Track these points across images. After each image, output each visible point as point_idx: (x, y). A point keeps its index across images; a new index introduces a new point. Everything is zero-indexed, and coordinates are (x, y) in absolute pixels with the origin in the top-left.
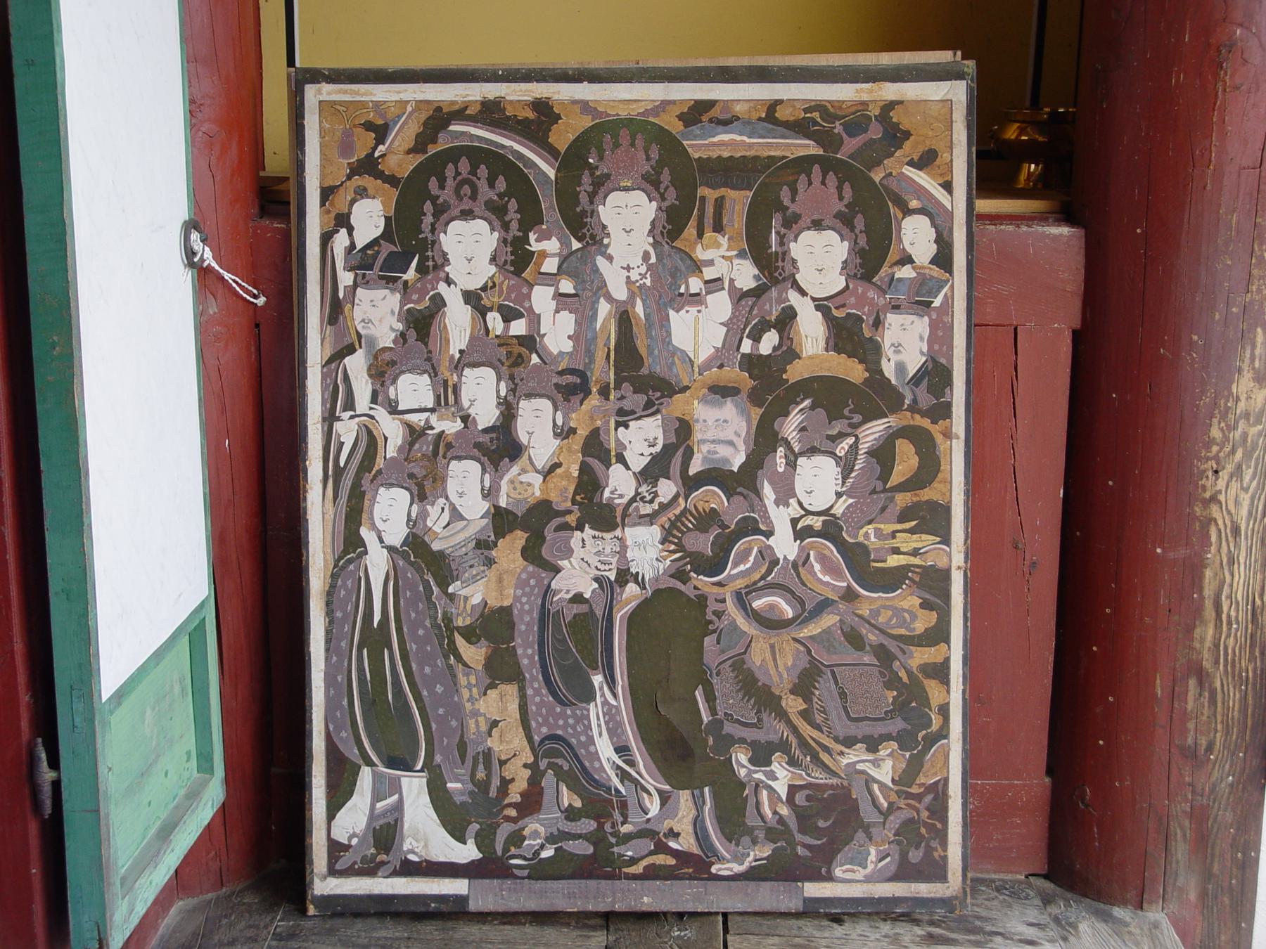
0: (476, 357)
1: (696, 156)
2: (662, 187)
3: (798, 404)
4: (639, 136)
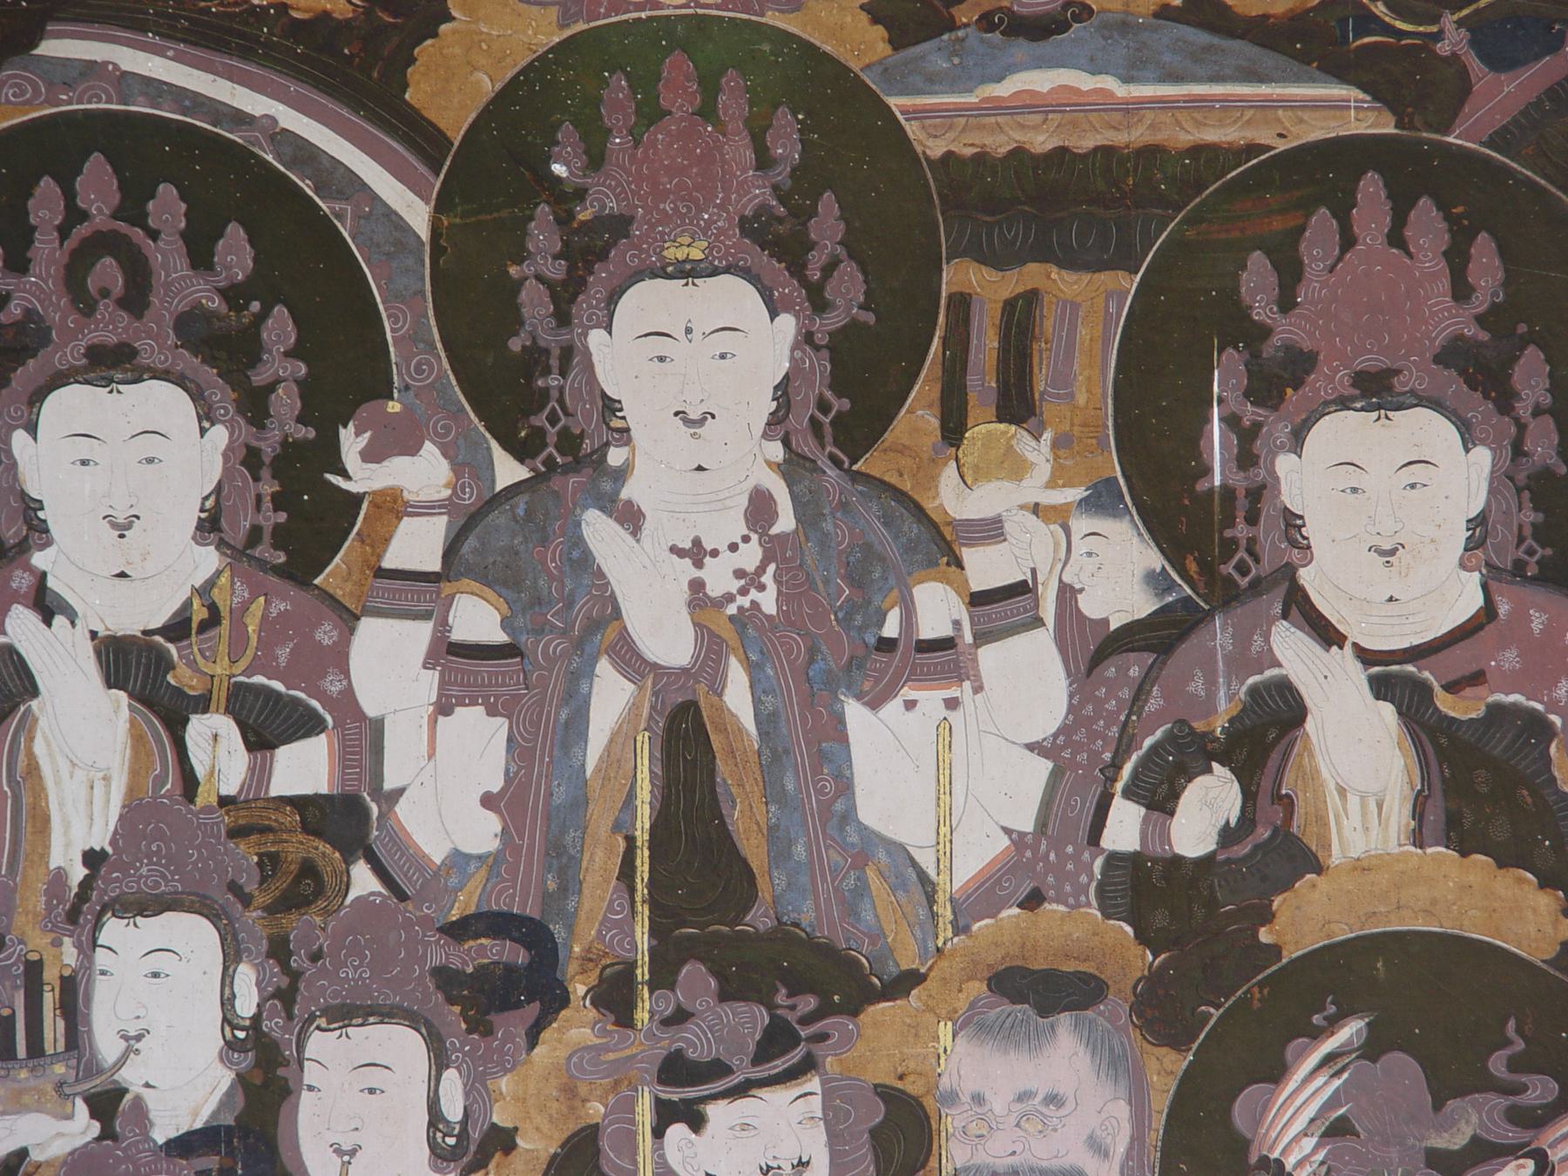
0: (146, 876)
1: (936, 149)
2: (815, 263)
3: (1317, 1034)
4: (731, 80)
